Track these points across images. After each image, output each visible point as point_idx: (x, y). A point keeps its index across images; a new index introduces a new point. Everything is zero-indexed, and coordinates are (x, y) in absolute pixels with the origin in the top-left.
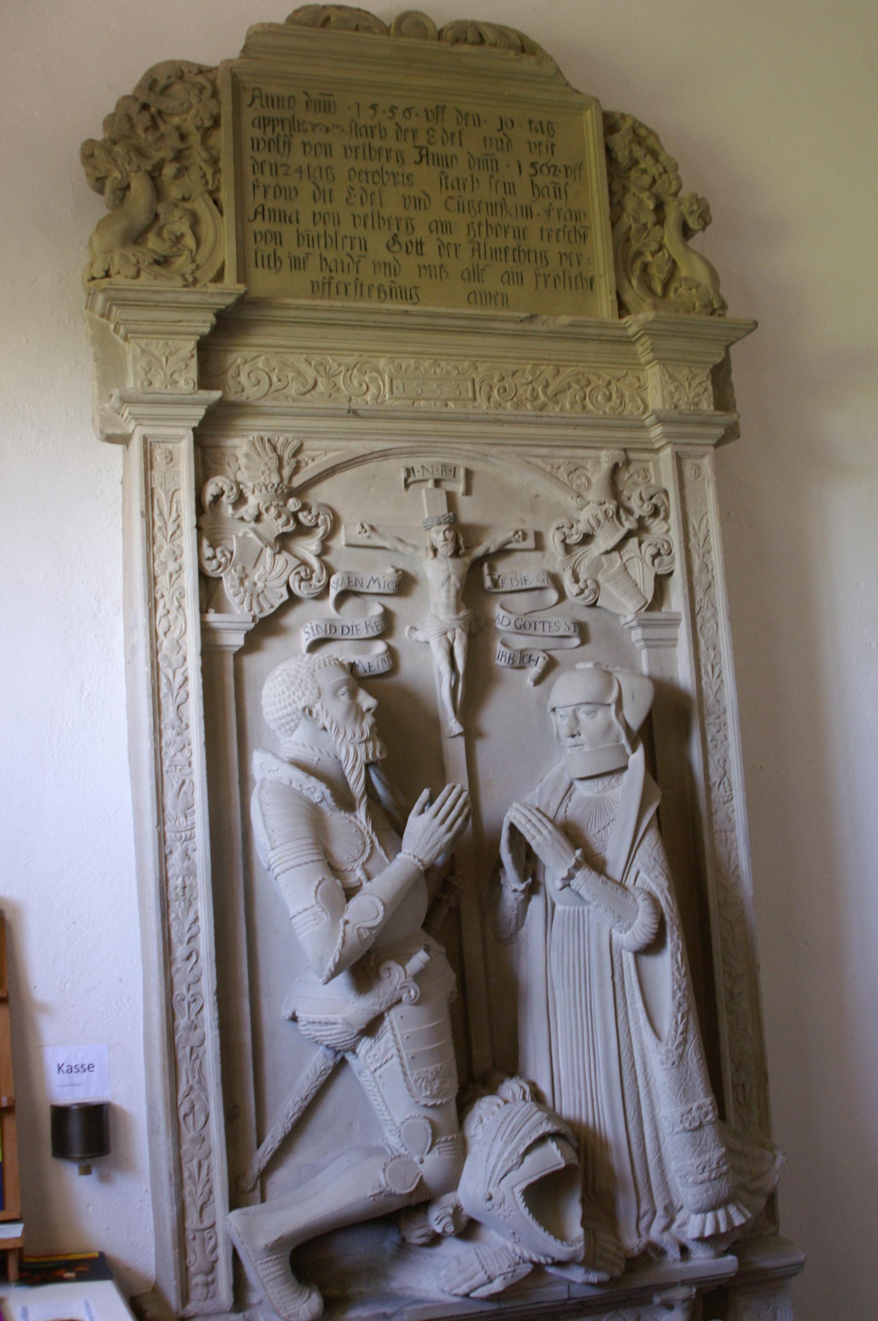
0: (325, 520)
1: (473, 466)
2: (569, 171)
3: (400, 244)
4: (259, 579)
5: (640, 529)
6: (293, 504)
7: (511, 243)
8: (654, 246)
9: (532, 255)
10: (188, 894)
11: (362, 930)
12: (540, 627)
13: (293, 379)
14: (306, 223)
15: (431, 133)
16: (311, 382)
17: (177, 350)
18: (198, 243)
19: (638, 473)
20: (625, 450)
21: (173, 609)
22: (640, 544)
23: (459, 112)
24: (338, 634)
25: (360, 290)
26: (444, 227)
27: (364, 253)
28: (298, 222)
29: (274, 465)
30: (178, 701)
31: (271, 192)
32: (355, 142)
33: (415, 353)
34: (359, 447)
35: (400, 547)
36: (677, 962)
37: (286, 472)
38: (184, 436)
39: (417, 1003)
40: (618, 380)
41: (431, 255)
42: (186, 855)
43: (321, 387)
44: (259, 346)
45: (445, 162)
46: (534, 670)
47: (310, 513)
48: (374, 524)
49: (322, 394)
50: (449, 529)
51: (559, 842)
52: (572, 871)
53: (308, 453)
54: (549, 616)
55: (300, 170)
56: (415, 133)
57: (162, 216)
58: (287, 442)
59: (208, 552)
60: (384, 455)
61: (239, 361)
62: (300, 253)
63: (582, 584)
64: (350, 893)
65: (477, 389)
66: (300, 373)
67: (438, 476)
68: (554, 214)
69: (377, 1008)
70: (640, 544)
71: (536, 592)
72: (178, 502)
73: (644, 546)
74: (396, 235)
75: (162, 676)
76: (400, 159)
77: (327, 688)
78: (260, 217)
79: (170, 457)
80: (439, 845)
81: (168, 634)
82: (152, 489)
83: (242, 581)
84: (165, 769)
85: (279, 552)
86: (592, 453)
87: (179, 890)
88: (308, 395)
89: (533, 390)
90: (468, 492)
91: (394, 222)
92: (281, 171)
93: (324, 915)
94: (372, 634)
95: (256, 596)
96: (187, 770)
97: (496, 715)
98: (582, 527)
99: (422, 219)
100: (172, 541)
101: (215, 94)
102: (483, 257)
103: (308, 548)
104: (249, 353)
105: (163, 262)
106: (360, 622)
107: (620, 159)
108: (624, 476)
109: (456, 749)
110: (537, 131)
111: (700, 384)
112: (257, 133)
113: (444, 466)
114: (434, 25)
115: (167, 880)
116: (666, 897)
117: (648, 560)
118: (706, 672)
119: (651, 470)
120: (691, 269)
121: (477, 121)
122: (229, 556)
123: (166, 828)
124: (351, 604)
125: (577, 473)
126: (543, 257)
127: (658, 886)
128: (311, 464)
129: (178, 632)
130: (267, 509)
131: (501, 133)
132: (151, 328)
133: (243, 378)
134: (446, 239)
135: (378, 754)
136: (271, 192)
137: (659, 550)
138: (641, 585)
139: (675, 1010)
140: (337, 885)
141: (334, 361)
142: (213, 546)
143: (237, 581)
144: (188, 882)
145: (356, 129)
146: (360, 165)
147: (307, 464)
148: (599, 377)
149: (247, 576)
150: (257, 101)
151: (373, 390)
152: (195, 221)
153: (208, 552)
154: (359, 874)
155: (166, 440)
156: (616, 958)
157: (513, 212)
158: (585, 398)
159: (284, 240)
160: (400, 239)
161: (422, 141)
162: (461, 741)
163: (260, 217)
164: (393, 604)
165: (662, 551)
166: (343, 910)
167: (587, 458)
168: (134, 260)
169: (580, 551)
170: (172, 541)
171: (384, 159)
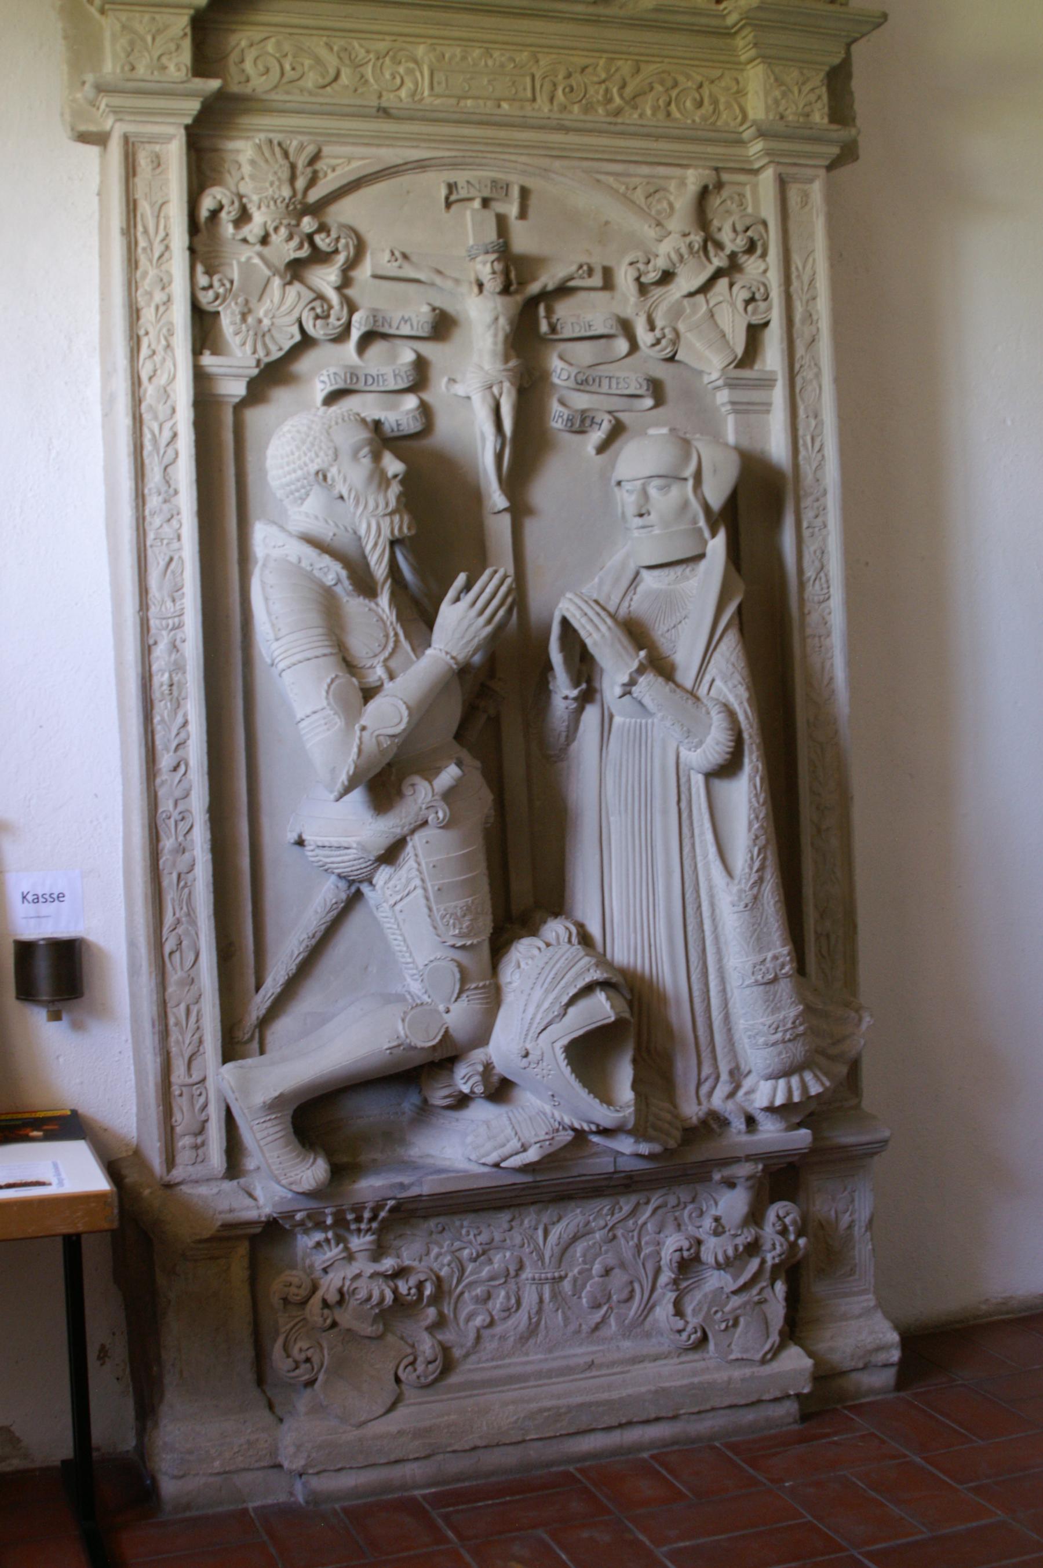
1: (530, 183)
4: (266, 315)
5: (732, 268)
6: (308, 224)
10: (175, 693)
12: (605, 382)
13: (311, 68)
16: (332, 72)
20: (717, 169)
21: (160, 349)
22: (731, 285)
29: (285, 174)
30: (166, 461)
34: (390, 155)
35: (438, 280)
37: (300, 183)
42: (174, 647)
43: (344, 79)
46: (597, 436)
47: (329, 235)
50: (498, 259)
51: (620, 642)
58: (302, 147)
59: (203, 280)
63: (658, 333)
64: (368, 693)
66: (318, 61)
67: (486, 193)
70: (731, 285)
71: (603, 341)
72: (167, 218)
73: (735, 288)
75: (146, 430)
79: (157, 162)
81: (154, 380)
83: (244, 316)
84: (148, 543)
85: (290, 283)
86: (677, 172)
87: (165, 687)
88: (328, 89)
89: (607, 91)
90: (523, 214)
94: (402, 385)
95: (261, 335)
96: (175, 545)
97: (548, 488)
98: (661, 263)
100: (159, 266)
103: (325, 278)
106: (388, 370)
108: (715, 202)
109: (500, 528)
113: (494, 182)
116: (745, 712)
117: (740, 306)
118: (805, 444)
119: (748, 195)
122: (228, 285)
124: (377, 349)
125: (657, 196)
127: (736, 696)
128: (331, 176)
133: (248, 66)
135: (405, 530)
137: (754, 294)
138: (729, 336)
139: (751, 843)
140: (353, 684)
141: (361, 46)
142: (209, 272)
147: (326, 175)
148: (688, 77)
149: (250, 311)
154: (380, 672)
155: (153, 139)
156: (683, 780)
158: (669, 104)
162: (506, 519)
164: (430, 350)
165: (757, 296)
166: (359, 714)
170: (159, 266)
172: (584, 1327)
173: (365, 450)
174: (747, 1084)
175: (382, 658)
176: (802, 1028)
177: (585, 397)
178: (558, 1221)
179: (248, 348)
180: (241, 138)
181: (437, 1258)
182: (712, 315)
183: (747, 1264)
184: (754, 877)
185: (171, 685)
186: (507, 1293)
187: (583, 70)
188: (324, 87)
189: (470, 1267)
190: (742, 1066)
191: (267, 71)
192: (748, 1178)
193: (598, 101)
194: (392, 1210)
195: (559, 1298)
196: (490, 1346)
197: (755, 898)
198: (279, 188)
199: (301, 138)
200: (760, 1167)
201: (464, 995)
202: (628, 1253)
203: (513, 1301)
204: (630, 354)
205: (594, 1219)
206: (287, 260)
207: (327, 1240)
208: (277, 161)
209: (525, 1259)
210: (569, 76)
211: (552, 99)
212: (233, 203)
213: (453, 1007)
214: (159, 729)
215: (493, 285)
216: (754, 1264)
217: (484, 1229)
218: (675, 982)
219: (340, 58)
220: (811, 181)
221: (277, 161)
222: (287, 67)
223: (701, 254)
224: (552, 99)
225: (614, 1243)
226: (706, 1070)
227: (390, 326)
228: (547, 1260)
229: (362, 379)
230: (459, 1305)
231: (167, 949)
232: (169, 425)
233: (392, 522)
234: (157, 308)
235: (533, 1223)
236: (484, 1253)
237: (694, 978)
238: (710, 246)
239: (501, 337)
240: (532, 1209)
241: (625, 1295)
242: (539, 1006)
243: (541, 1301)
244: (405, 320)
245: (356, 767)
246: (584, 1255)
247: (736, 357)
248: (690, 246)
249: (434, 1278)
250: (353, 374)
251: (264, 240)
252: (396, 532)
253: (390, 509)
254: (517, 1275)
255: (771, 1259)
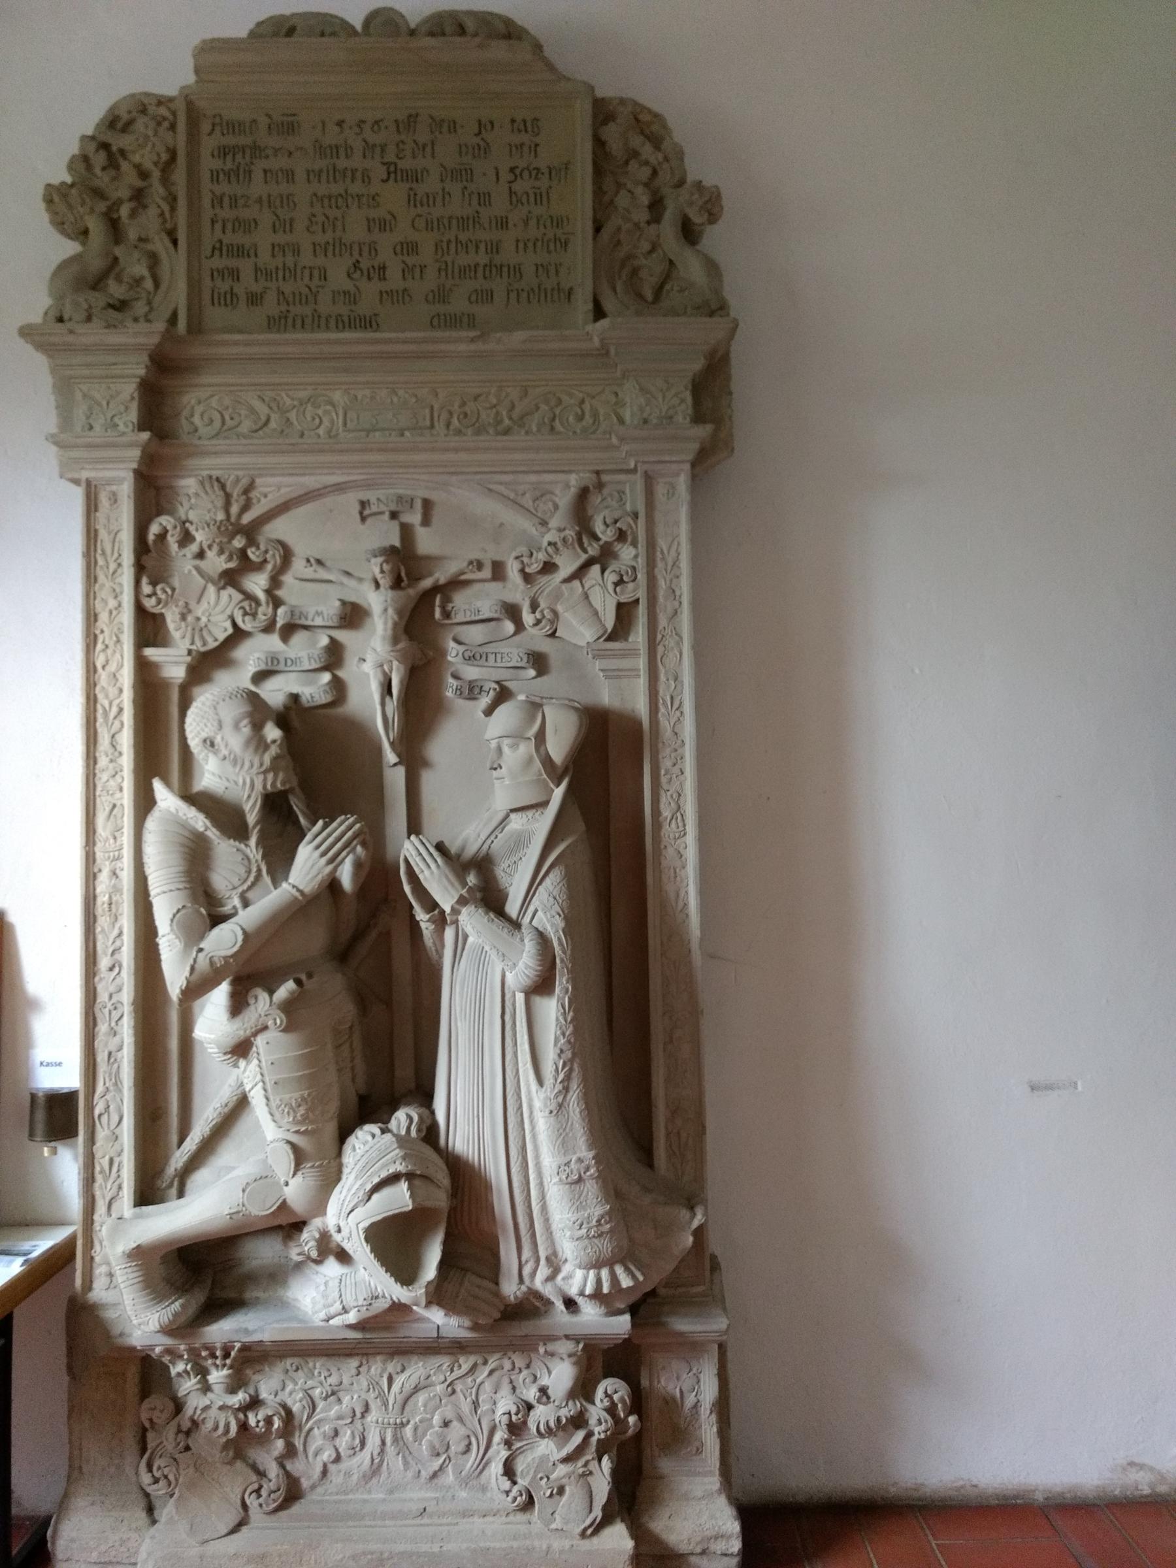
0: (274, 555)
1: (434, 496)
2: (554, 173)
3: (361, 270)
4: (203, 614)
5: (605, 557)
6: (238, 542)
7: (482, 258)
8: (646, 246)
9: (505, 269)
10: (114, 910)
11: (216, 959)
12: (491, 657)
13: (246, 416)
14: (265, 258)
15: (401, 146)
16: (264, 418)
17: (118, 393)
18: (157, 284)
19: (611, 495)
20: (598, 473)
21: (111, 644)
22: (603, 571)
23: (432, 118)
24: (281, 667)
25: (318, 322)
26: (411, 248)
27: (323, 283)
28: (256, 255)
29: (220, 503)
30: (113, 731)
31: (229, 226)
32: (320, 164)
33: (368, 383)
34: (311, 482)
35: (345, 580)
36: (564, 1008)
37: (235, 509)
38: (124, 479)
39: (286, 1030)
40: (593, 397)
41: (395, 279)
42: (114, 874)
43: (273, 424)
44: (210, 385)
45: (415, 177)
46: (485, 701)
47: (258, 548)
48: (318, 557)
49: (275, 430)
50: (386, 561)
51: (447, 877)
52: (457, 907)
53: (261, 489)
54: (503, 648)
55: (260, 200)
56: (383, 148)
57: (121, 260)
58: (238, 480)
59: (146, 589)
60: (339, 488)
61: (193, 402)
62: (256, 288)
63: (538, 615)
64: (216, 920)
65: (436, 415)
66: (252, 411)
67: (393, 507)
68: (533, 223)
69: (242, 1034)
70: (603, 571)
71: (493, 623)
72: (120, 542)
73: (606, 573)
74: (358, 261)
75: (99, 707)
76: (366, 178)
77: (228, 721)
78: (217, 252)
79: (114, 499)
80: (320, 877)
81: (107, 668)
82: (96, 531)
83: (183, 617)
84: (97, 793)
85: (223, 588)
86: (561, 477)
87: (106, 906)
88: (261, 432)
89: (497, 413)
90: (426, 521)
91: (356, 248)
92: (241, 202)
93: (177, 941)
94: (315, 666)
95: (200, 631)
96: (118, 795)
97: (445, 746)
98: (541, 556)
99: (385, 242)
100: (113, 580)
101: (173, 127)
102: (450, 276)
103: (257, 584)
104: (203, 393)
105: (121, 306)
106: (303, 654)
107: (614, 153)
108: (595, 499)
109: (395, 778)
110: (520, 131)
111: (676, 395)
112: (217, 164)
113: (400, 499)
114: (406, 22)
115: (95, 897)
116: (559, 939)
117: (610, 587)
118: (664, 703)
119: (628, 491)
120: (692, 268)
121: (453, 127)
122: (170, 592)
123: (96, 849)
124: (299, 638)
125: (544, 499)
126: (517, 271)
127: (552, 925)
128: (263, 500)
129: (115, 665)
130: (210, 547)
131: (479, 137)
132: (86, 372)
133: (196, 420)
134: (410, 261)
135: (279, 785)
136: (229, 226)
137: (622, 576)
138: (601, 614)
139: (556, 1057)
140: (201, 914)
141: (288, 396)
142: (154, 583)
143: (179, 616)
144: (114, 899)
145: (320, 150)
146: (322, 189)
147: (259, 501)
148: (571, 395)
149: (190, 611)
150: (218, 129)
151: (326, 423)
152: (154, 261)
153: (146, 589)
154: (236, 902)
155: (109, 482)
156: (508, 997)
157: (487, 226)
158: (553, 419)
159: (242, 275)
160: (361, 265)
161: (390, 157)
162: (401, 771)
163: (217, 252)
164: (342, 636)
165: (625, 578)
166: (202, 937)
167: (557, 482)
168: (85, 306)
169: (543, 580)
170: (113, 580)
171: (348, 180)
172: (423, 1472)
173: (245, 722)
174: (566, 1269)
175: (240, 890)
176: (608, 1226)
177: (477, 670)
178: (402, 1371)
179: (187, 641)
180: (190, 476)
181: (291, 1394)
182: (586, 596)
183: (572, 1435)
184: (559, 1087)
185: (110, 904)
186: (353, 1433)
187: (476, 398)
188: (256, 431)
189: (321, 1405)
190: (560, 1254)
191: (212, 421)
192: (570, 1356)
193: (489, 424)
194: (241, 1350)
195: (401, 1443)
196: (336, 1477)
197: (560, 1105)
198: (215, 514)
199: (237, 473)
200: (581, 1346)
201: (300, 1173)
202: (466, 1407)
203: (357, 1441)
204: (515, 634)
205: (435, 1374)
206: (221, 570)
207: (186, 1371)
208: (214, 491)
209: (370, 1403)
210: (463, 404)
211: (448, 425)
212: (175, 527)
213: (291, 1182)
214: (100, 938)
215: (385, 582)
216: (579, 1437)
217: (334, 1370)
218: (498, 1177)
219: (271, 408)
220: (678, 475)
221: (214, 491)
222: (227, 418)
223: (577, 546)
224: (448, 425)
225: (453, 1397)
226: (527, 1253)
227: (306, 618)
228: (391, 1407)
229: (282, 662)
230: (309, 1439)
231: (97, 1112)
232: (117, 702)
233: (265, 780)
234: (111, 612)
235: (379, 1371)
236: (333, 1393)
237: (514, 1170)
238: (585, 540)
239: (390, 625)
240: (379, 1358)
241: (462, 1447)
242: (349, 1190)
243: (383, 1443)
244: (318, 613)
245: (188, 982)
246: (425, 1406)
247: (606, 632)
248: (564, 540)
249: (283, 1413)
250: (274, 658)
251: (201, 555)
252: (269, 787)
253: (264, 768)
254: (363, 1417)
255: (599, 1432)
